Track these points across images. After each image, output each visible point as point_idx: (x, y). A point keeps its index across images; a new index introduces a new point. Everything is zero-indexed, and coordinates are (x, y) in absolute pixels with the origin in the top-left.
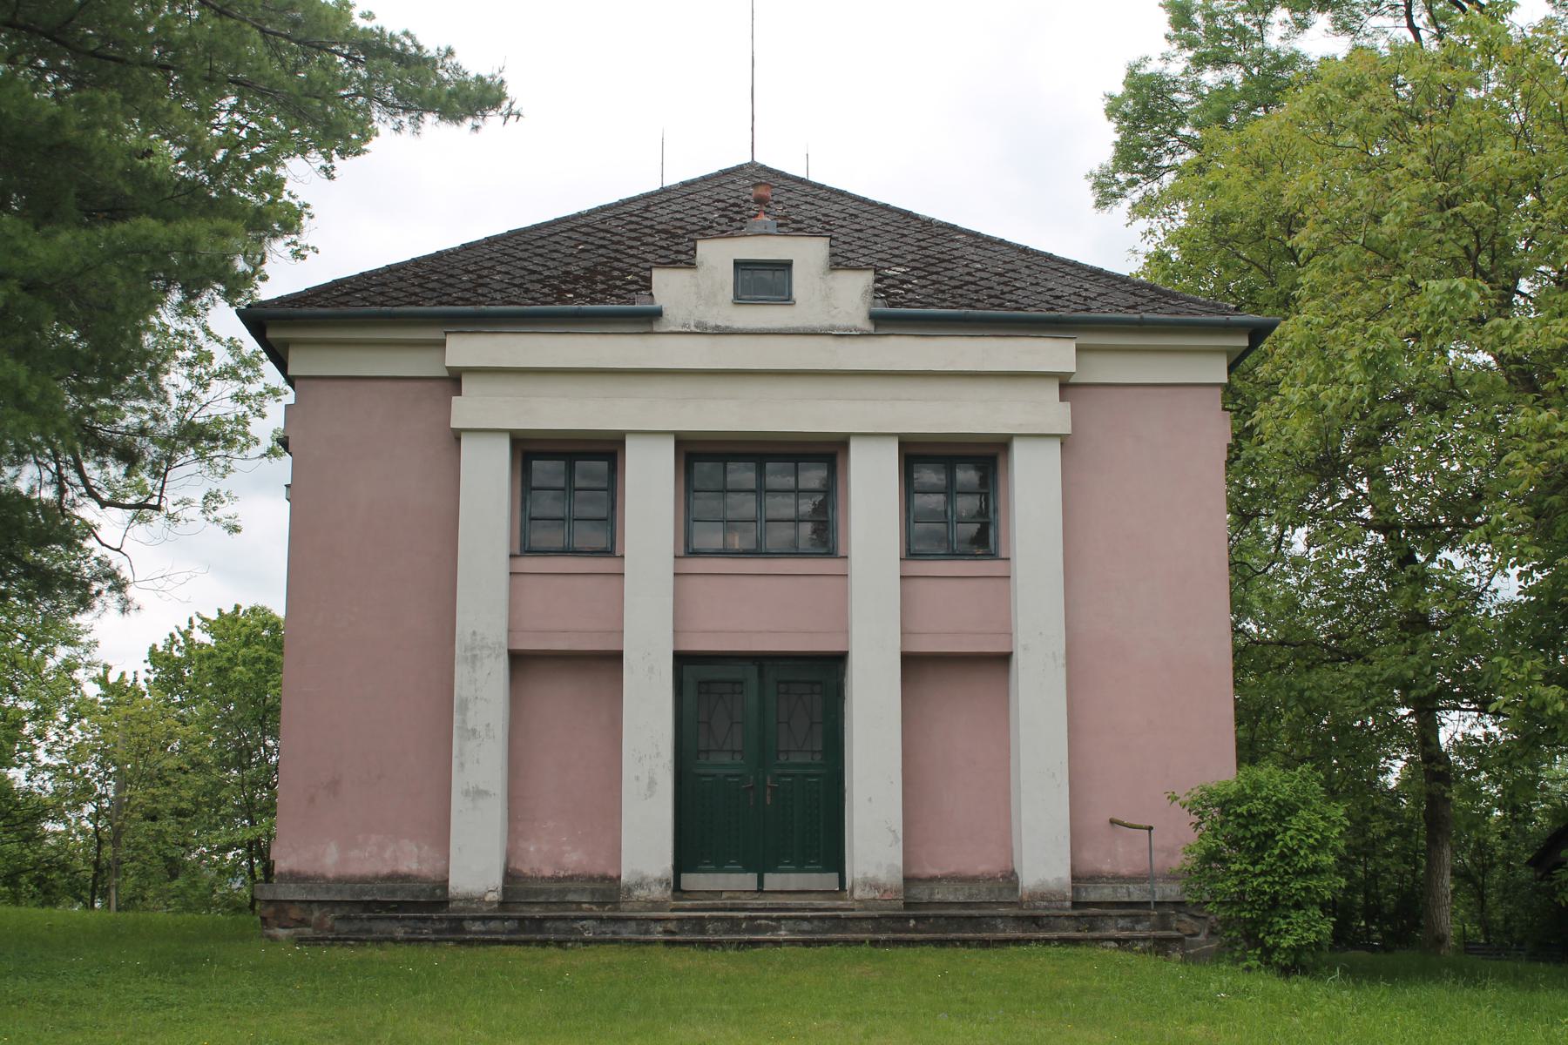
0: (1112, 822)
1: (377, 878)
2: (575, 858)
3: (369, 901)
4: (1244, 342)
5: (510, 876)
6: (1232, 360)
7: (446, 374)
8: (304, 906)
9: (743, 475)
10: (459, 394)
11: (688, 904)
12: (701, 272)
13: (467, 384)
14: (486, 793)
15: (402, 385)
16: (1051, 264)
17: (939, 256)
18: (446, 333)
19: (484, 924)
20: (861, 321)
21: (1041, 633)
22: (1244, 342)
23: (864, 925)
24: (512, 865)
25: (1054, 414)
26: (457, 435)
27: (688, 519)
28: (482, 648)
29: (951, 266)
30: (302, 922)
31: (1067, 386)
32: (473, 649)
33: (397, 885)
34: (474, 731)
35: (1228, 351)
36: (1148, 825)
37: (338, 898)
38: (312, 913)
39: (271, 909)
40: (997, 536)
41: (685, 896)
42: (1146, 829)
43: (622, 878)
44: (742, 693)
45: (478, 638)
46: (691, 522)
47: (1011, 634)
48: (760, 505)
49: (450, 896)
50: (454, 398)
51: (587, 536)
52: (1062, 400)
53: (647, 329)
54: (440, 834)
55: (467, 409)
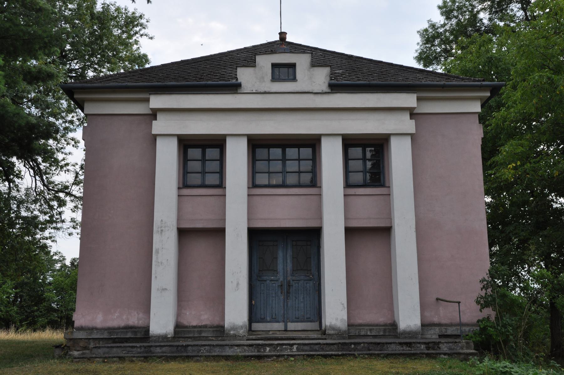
0: (438, 299)
1: (119, 328)
2: (206, 317)
3: (115, 338)
4: (488, 94)
5: (178, 327)
6: (483, 102)
7: (150, 112)
8: (87, 341)
9: (276, 152)
10: (156, 119)
11: (254, 337)
12: (257, 68)
13: (159, 116)
14: (166, 289)
15: (133, 118)
16: (401, 68)
17: (357, 67)
18: (150, 94)
19: (161, 349)
20: (325, 88)
21: (404, 218)
22: (488, 94)
23: (332, 347)
24: (179, 320)
25: (409, 125)
26: (155, 137)
27: (253, 172)
28: (165, 227)
29: (361, 70)
30: (85, 348)
31: (413, 113)
32: (161, 227)
33: (137, 330)
34: (162, 263)
35: (480, 98)
36: (458, 300)
37: (102, 337)
38: (90, 344)
39: (72, 342)
40: (384, 178)
41: (254, 333)
42: (457, 302)
43: (225, 326)
44: (277, 245)
45: (164, 222)
46: (255, 173)
47: (391, 219)
48: (284, 165)
49: (150, 335)
50: (153, 122)
51: (212, 179)
52: (411, 119)
53: (235, 92)
54: (147, 308)
55: (158, 126)
